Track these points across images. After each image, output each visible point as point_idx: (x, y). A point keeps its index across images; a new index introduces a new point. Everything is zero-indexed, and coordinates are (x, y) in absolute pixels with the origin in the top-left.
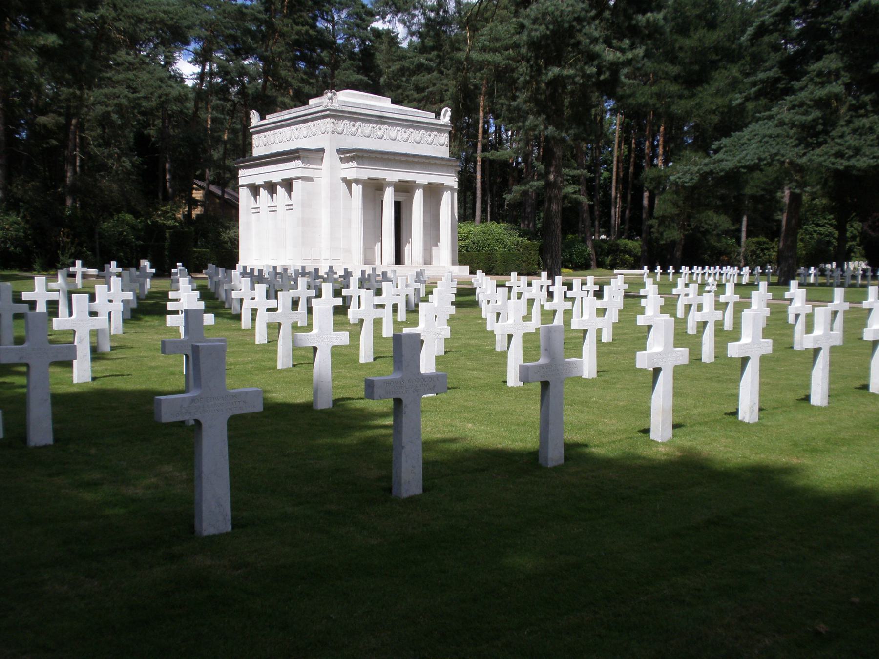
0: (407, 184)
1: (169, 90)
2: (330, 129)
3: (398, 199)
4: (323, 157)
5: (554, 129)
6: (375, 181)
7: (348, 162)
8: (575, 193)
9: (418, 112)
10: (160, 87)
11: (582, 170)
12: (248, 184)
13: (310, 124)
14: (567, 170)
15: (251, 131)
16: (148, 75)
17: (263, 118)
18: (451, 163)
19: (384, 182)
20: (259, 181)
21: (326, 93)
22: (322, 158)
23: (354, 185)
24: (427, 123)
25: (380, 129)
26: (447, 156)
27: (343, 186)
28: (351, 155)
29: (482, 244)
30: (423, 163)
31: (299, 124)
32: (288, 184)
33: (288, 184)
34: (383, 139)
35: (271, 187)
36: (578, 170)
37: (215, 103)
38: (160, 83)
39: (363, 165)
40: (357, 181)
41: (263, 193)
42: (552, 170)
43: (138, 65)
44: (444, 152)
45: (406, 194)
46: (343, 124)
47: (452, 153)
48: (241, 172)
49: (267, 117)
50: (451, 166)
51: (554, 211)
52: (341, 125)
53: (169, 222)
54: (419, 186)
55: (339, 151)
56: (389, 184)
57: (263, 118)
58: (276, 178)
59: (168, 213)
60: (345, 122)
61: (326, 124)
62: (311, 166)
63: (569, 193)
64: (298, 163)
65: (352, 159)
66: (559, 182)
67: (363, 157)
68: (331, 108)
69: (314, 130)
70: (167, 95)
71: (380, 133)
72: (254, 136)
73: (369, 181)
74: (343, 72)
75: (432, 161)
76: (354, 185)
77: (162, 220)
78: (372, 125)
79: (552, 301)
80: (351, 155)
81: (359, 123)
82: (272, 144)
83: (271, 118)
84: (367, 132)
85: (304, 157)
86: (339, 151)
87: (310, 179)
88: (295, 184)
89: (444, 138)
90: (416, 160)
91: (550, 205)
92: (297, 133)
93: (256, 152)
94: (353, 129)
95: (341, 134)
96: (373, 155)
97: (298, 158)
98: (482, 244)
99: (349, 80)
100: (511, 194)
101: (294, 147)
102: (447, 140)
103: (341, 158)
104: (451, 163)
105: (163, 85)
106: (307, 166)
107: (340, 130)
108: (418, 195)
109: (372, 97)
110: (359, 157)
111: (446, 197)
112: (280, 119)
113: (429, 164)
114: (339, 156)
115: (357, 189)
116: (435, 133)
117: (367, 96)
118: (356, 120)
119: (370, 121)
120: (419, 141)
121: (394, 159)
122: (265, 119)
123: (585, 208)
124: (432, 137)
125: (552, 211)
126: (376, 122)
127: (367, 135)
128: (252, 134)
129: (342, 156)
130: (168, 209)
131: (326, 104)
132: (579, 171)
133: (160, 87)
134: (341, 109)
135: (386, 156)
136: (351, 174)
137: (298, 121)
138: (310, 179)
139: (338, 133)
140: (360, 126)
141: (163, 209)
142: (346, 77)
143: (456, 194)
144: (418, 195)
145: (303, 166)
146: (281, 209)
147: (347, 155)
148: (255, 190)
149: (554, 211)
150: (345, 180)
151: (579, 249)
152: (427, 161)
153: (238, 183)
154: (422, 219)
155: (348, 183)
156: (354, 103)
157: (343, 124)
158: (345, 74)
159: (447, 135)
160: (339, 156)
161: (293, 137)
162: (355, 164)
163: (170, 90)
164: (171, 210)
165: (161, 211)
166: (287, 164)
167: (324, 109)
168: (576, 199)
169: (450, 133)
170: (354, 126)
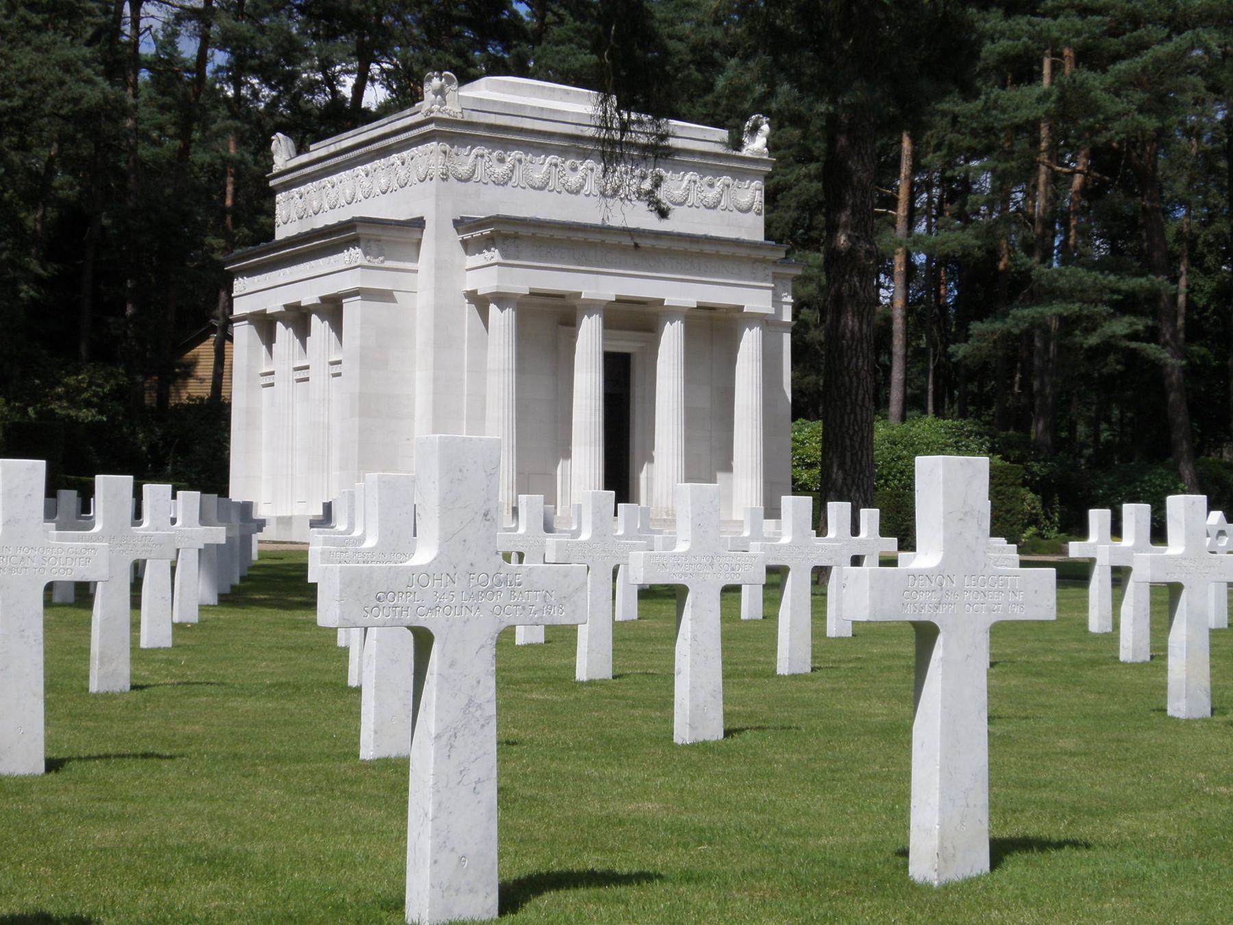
0: (648, 309)
1: (80, 88)
2: (437, 170)
3: (621, 346)
4: (420, 240)
5: (796, 92)
6: (558, 302)
7: (481, 252)
8: (1134, 336)
9: (683, 127)
10: (62, 83)
11: (1152, 277)
12: (252, 314)
13: (395, 158)
14: (1112, 277)
15: (272, 183)
16: (34, 55)
17: (301, 149)
18: (761, 254)
19: (576, 302)
20: (274, 303)
21: (430, 79)
22: (418, 244)
23: (493, 308)
24: (703, 154)
25: (574, 169)
26: (759, 237)
27: (469, 311)
28: (487, 232)
29: (885, 472)
30: (686, 254)
31: (372, 160)
32: (332, 308)
33: (332, 308)
34: (582, 195)
35: (298, 318)
36: (1141, 275)
37: (223, 125)
38: (60, 74)
39: (518, 258)
40: (501, 299)
41: (283, 333)
42: (844, 217)
43: (14, 34)
44: (752, 228)
45: (639, 334)
46: (472, 156)
47: (769, 229)
48: (240, 285)
49: (312, 147)
50: (764, 261)
51: (849, 335)
52: (466, 159)
53: (81, 414)
54: (673, 313)
55: (461, 224)
56: (591, 307)
57: (301, 149)
58: (309, 296)
59: (80, 391)
60: (478, 150)
61: (429, 156)
62: (388, 264)
63: (1114, 336)
64: (354, 255)
65: (488, 243)
66: (862, 253)
67: (516, 237)
68: (440, 115)
69: (402, 172)
70: (76, 101)
71: (574, 179)
72: (279, 197)
73: (536, 300)
74: (555, 49)
75: (708, 249)
76: (493, 308)
77: (65, 408)
78: (552, 158)
79: (141, 524)
80: (487, 232)
81: (516, 154)
82: (316, 214)
83: (319, 150)
84: (538, 176)
85: (369, 240)
86: (461, 224)
87: (385, 296)
88: (352, 309)
89: (752, 193)
90: (663, 244)
91: (839, 321)
92: (366, 183)
93: (281, 234)
94: (500, 170)
95: (467, 180)
96: (546, 233)
97: (354, 242)
98: (885, 472)
99: (566, 66)
100: (966, 341)
101: (344, 215)
102: (759, 197)
103: (465, 243)
104: (761, 254)
105: (67, 78)
106: (376, 262)
107: (463, 170)
108: (672, 337)
109: (567, 92)
110: (506, 237)
111: (750, 343)
112: (332, 149)
113: (702, 255)
114: (459, 238)
115: (502, 319)
116: (726, 179)
117: (553, 90)
118: (507, 145)
119: (545, 150)
120: (679, 200)
121: (603, 243)
122: (307, 151)
123: (1174, 378)
124: (717, 189)
125: (843, 336)
126: (563, 152)
127: (538, 184)
128: (272, 193)
129: (467, 236)
130: (80, 382)
131: (428, 107)
132: (1143, 280)
133: (62, 83)
134: (466, 119)
135: (580, 236)
136: (486, 283)
137: (369, 153)
138: (385, 296)
139: (460, 180)
140: (520, 161)
141: (71, 380)
142: (560, 61)
143: (787, 339)
144: (672, 337)
145: (366, 263)
146: (320, 373)
147: (477, 234)
148: (265, 324)
149: (849, 335)
150: (472, 297)
151: (1154, 486)
152: (695, 248)
153: (231, 313)
154: (681, 399)
155: (481, 302)
156: (505, 104)
157: (472, 156)
158: (558, 53)
159: (758, 184)
160: (459, 238)
161: (360, 196)
162: (494, 255)
163: (80, 88)
164: (90, 384)
165: (66, 385)
166: (333, 258)
167: (423, 118)
168: (1134, 352)
169: (768, 177)
170: (502, 161)
